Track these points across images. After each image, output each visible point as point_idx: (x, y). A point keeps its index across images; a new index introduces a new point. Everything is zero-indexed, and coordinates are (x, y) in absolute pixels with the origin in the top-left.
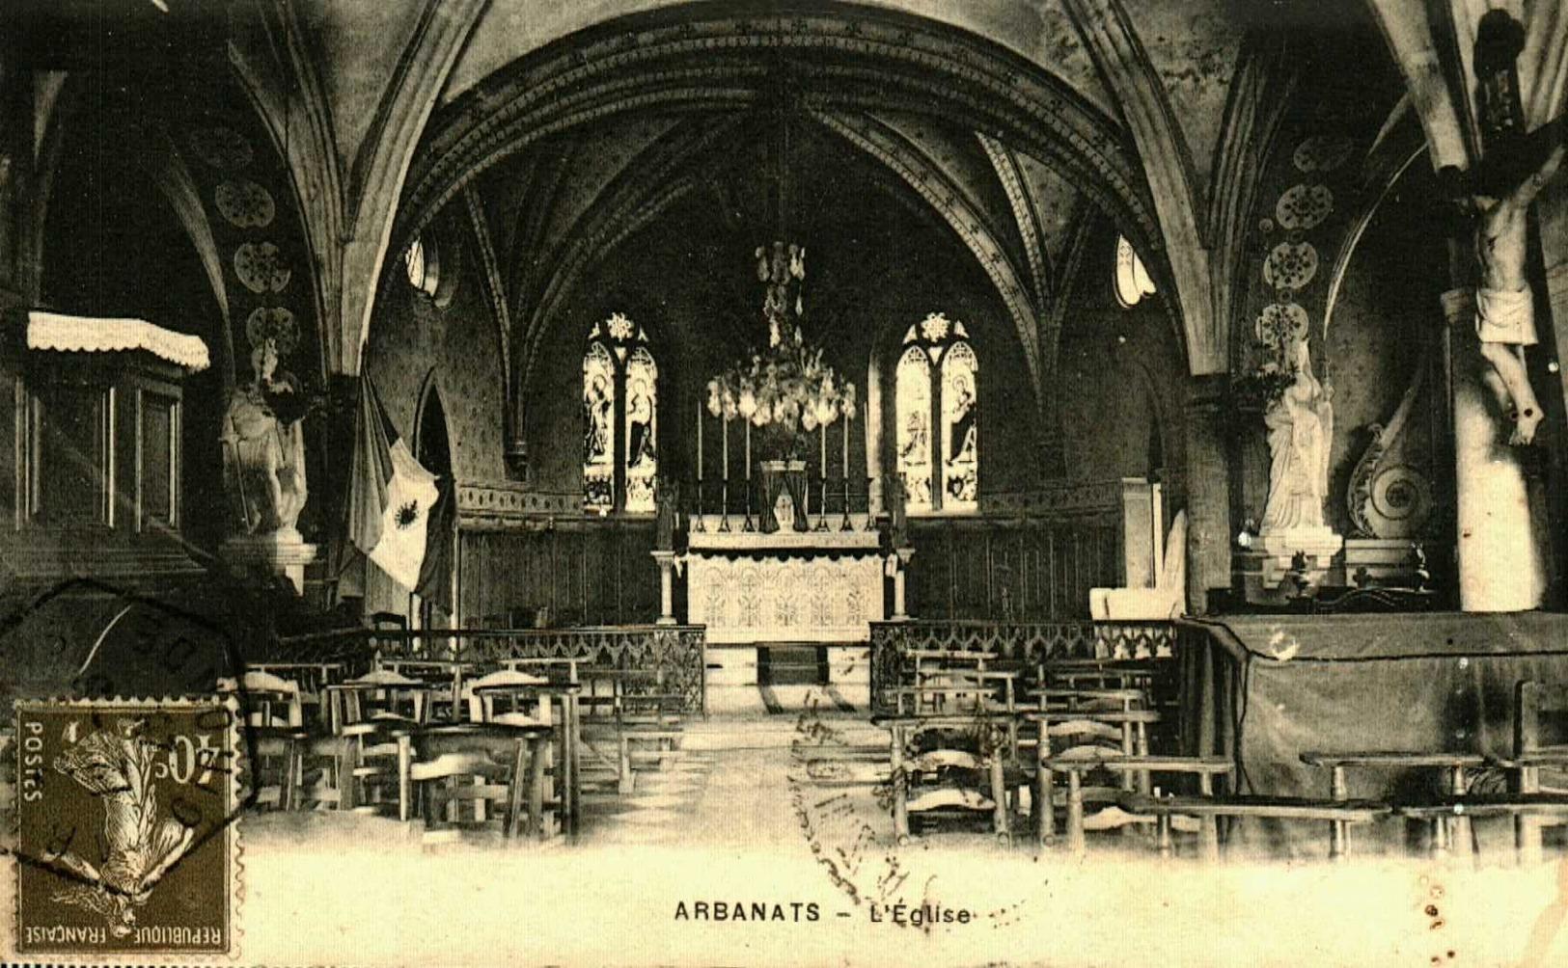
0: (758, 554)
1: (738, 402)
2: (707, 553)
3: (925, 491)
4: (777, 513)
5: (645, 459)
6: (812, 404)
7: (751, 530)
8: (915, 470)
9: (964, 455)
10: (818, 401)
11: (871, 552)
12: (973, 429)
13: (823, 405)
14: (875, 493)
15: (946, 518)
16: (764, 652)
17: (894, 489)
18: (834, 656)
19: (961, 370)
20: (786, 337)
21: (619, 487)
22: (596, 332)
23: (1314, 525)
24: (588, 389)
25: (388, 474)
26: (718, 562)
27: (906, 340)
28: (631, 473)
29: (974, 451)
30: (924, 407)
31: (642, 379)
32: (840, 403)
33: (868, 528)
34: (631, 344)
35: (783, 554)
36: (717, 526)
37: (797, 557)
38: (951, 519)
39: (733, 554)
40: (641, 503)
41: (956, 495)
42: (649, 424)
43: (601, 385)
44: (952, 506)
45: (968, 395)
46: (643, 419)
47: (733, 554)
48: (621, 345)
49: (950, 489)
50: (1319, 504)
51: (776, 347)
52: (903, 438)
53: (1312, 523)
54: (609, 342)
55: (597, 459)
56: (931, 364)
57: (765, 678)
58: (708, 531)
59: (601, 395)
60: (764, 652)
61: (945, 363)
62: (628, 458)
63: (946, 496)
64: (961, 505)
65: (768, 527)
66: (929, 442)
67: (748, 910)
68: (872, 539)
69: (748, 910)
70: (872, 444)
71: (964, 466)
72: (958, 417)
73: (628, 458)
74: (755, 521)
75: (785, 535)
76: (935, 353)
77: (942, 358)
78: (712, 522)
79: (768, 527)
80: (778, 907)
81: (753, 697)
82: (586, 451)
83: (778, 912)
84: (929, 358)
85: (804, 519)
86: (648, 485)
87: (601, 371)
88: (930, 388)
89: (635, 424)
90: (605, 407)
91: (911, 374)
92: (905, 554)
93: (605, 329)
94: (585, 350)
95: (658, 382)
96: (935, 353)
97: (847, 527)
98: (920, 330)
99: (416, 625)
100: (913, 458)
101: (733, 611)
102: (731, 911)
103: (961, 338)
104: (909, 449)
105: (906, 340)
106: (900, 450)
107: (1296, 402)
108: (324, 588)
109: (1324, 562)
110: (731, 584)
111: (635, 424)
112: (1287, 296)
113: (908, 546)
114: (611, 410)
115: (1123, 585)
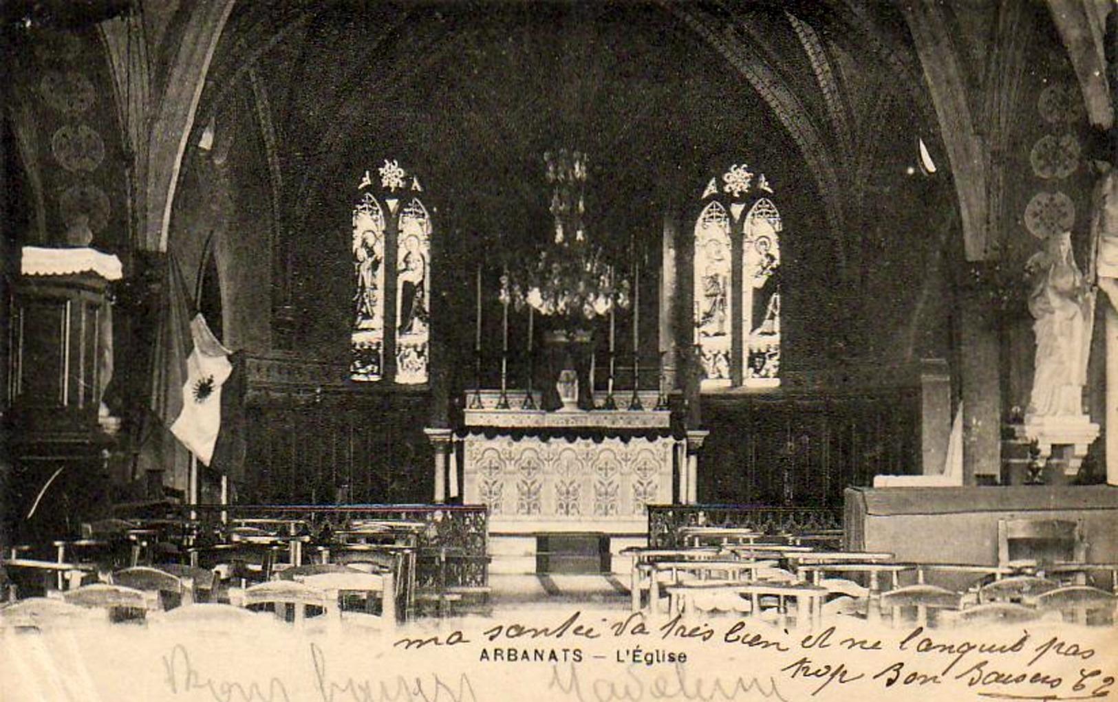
0: (545, 434)
1: (526, 296)
2: (491, 432)
3: (723, 365)
4: (560, 388)
5: (417, 324)
6: (591, 297)
7: (532, 407)
8: (712, 342)
9: (767, 325)
10: (597, 296)
11: (665, 433)
12: (776, 297)
13: (601, 300)
14: (668, 371)
15: (744, 396)
16: (543, 541)
17: (689, 362)
18: (616, 546)
19: (764, 229)
20: (570, 236)
21: (388, 356)
22: (367, 181)
23: (1073, 414)
24: (357, 244)
25: (189, 349)
26: (500, 443)
27: (706, 194)
28: (402, 340)
29: (777, 319)
30: (724, 269)
31: (415, 234)
32: (617, 297)
33: (658, 407)
34: (404, 195)
35: (570, 434)
36: (496, 401)
37: (612, 437)
38: (749, 397)
39: (516, 434)
40: (412, 373)
41: (757, 371)
42: (421, 283)
43: (371, 241)
44: (753, 383)
45: (772, 259)
46: (414, 277)
47: (516, 434)
48: (392, 197)
49: (751, 364)
50: (1079, 391)
51: (561, 244)
52: (702, 304)
53: (1069, 412)
54: (381, 193)
55: (365, 324)
56: (732, 223)
57: (543, 567)
58: (485, 409)
59: (371, 252)
60: (543, 541)
61: (747, 224)
62: (398, 323)
63: (747, 372)
64: (762, 382)
65: (551, 404)
66: (729, 310)
67: (531, 654)
68: (663, 418)
69: (531, 654)
70: (666, 307)
71: (765, 339)
72: (760, 282)
73: (398, 323)
74: (537, 397)
75: (568, 415)
76: (737, 209)
77: (744, 215)
78: (489, 399)
79: (551, 404)
80: (553, 652)
81: (534, 584)
82: (353, 311)
83: (553, 655)
84: (730, 215)
85: (590, 397)
86: (420, 354)
87: (372, 226)
88: (730, 254)
89: (406, 284)
90: (375, 265)
91: (710, 234)
92: (698, 436)
93: (377, 178)
94: (355, 199)
95: (432, 239)
96: (737, 209)
97: (636, 406)
98: (721, 184)
99: (194, 502)
100: (711, 328)
101: (510, 493)
102: (520, 655)
103: (765, 194)
104: (708, 315)
105: (706, 194)
106: (698, 317)
107: (1061, 294)
108: (125, 461)
109: (1081, 450)
110: (510, 467)
111: (406, 284)
112: (1051, 187)
113: (701, 428)
114: (382, 267)
115: (921, 473)
